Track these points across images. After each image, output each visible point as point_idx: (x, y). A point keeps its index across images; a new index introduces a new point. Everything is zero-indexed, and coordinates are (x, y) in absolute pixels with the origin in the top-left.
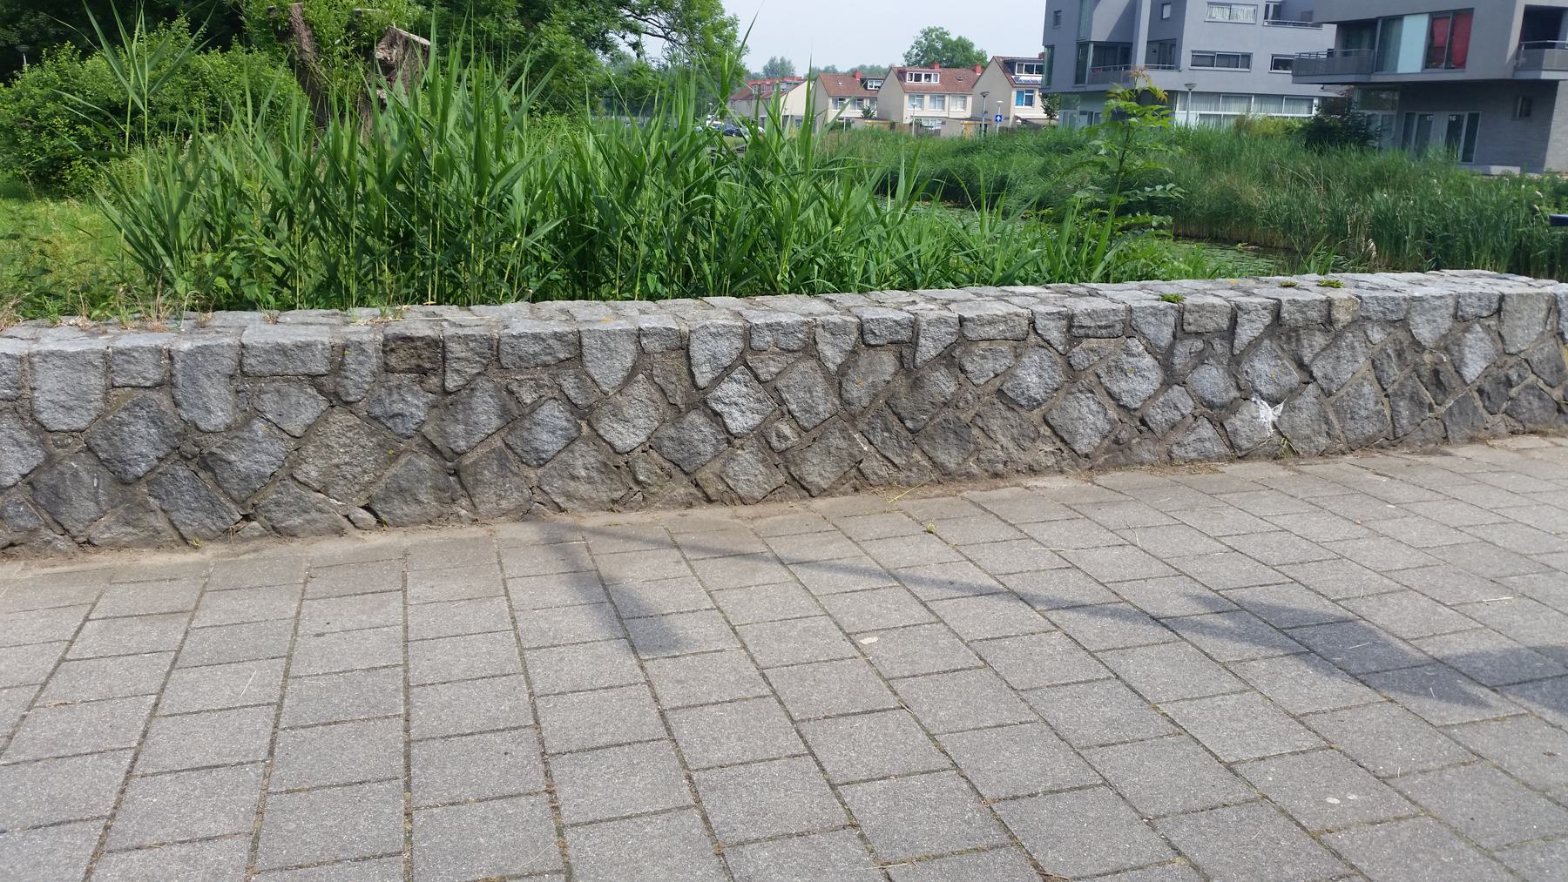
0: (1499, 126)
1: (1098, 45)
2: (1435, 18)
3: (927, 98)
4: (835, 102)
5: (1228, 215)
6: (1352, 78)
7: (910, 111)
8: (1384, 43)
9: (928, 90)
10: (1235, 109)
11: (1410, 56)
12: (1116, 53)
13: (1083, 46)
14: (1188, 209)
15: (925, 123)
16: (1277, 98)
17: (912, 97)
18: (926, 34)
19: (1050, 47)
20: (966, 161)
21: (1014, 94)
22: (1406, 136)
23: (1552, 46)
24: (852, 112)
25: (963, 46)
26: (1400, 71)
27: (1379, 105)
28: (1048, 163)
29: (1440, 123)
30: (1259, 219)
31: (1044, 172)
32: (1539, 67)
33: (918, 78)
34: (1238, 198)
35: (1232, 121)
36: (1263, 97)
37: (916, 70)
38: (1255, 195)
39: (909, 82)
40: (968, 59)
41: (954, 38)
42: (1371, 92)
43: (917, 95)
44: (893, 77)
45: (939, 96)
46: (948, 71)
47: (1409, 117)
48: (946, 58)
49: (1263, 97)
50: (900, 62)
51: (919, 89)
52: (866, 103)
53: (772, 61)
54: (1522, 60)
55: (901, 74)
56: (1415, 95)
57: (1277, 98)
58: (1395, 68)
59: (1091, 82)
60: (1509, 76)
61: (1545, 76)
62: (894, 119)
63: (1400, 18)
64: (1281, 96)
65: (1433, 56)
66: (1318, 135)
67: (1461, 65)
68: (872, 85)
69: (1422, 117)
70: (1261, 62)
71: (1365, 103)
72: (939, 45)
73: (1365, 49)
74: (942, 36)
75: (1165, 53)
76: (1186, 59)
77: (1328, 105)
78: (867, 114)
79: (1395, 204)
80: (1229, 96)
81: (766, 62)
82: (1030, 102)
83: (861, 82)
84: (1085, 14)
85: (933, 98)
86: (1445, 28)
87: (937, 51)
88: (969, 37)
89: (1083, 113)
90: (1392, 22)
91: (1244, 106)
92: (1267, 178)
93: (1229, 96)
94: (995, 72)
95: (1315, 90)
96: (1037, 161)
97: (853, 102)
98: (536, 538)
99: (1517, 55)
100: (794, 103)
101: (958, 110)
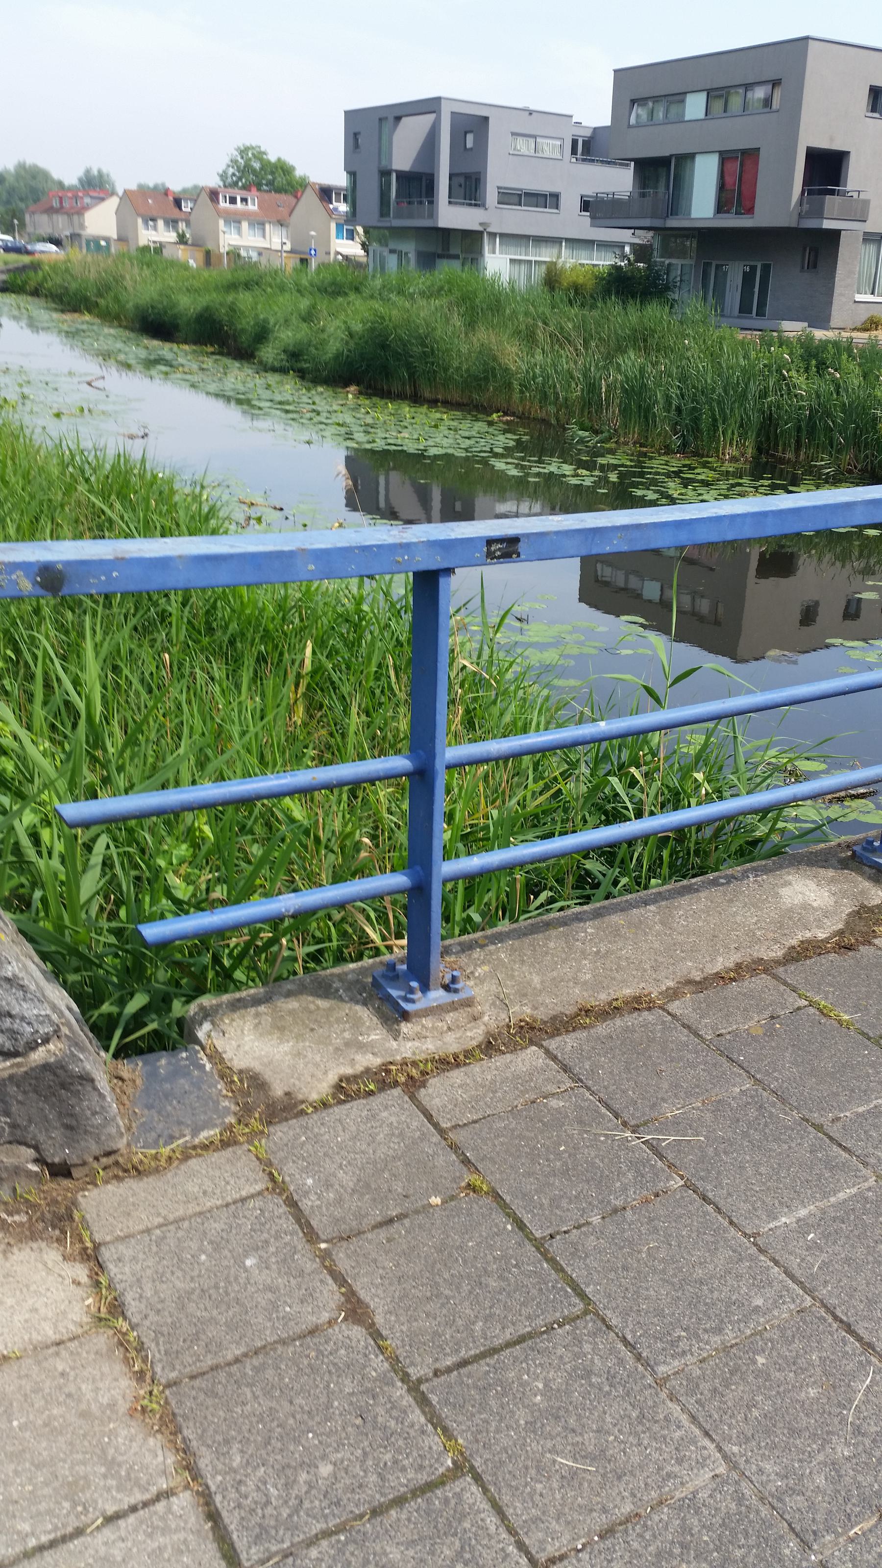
0: (787, 280)
1: (401, 175)
2: (725, 157)
3: (245, 225)
4: (146, 222)
5: (486, 379)
6: (647, 223)
7: (229, 239)
8: (678, 179)
9: (246, 216)
10: (546, 255)
11: (702, 204)
12: (418, 184)
13: (385, 173)
14: (446, 370)
15: (243, 253)
16: (588, 244)
17: (227, 222)
18: (243, 152)
19: (352, 174)
20: (230, 298)
21: (333, 226)
22: (705, 286)
23: (832, 193)
24: (164, 235)
25: (283, 169)
26: (695, 214)
27: (682, 254)
28: (314, 306)
29: (735, 274)
30: (516, 385)
31: (308, 317)
32: (821, 216)
33: (233, 201)
34: (495, 359)
35: (543, 268)
36: (574, 243)
37: (230, 192)
38: (512, 355)
39: (223, 205)
40: (289, 184)
41: (273, 158)
42: (674, 238)
43: (234, 220)
44: (205, 198)
45: (258, 223)
46: (266, 196)
47: (707, 265)
48: (265, 180)
49: (574, 243)
50: (214, 182)
51: (236, 213)
52: (182, 226)
53: (88, 172)
54: (806, 207)
55: (214, 195)
56: (710, 241)
57: (588, 244)
58: (690, 214)
59: (398, 216)
60: (794, 224)
61: (827, 224)
62: (210, 246)
63: (692, 156)
64: (527, 237)
65: (721, 207)
66: (621, 285)
67: (750, 211)
68: (186, 207)
69: (718, 267)
70: (570, 203)
71: (667, 252)
72: (257, 165)
73: (661, 189)
74: (260, 155)
75: (469, 187)
76: (491, 196)
77: (642, 252)
78: (182, 239)
79: (642, 370)
80: (541, 240)
81: (80, 173)
82: (351, 236)
83: (168, 204)
84: (385, 137)
85: (251, 225)
86: (734, 167)
87: (254, 171)
88: (290, 159)
89: (392, 251)
90: (686, 159)
91: (555, 251)
92: (529, 338)
93: (541, 240)
94: (310, 199)
95: (625, 236)
96: (304, 304)
97: (167, 223)
98: (527, 504)
99: (801, 202)
100: (101, 221)
101: (275, 239)
